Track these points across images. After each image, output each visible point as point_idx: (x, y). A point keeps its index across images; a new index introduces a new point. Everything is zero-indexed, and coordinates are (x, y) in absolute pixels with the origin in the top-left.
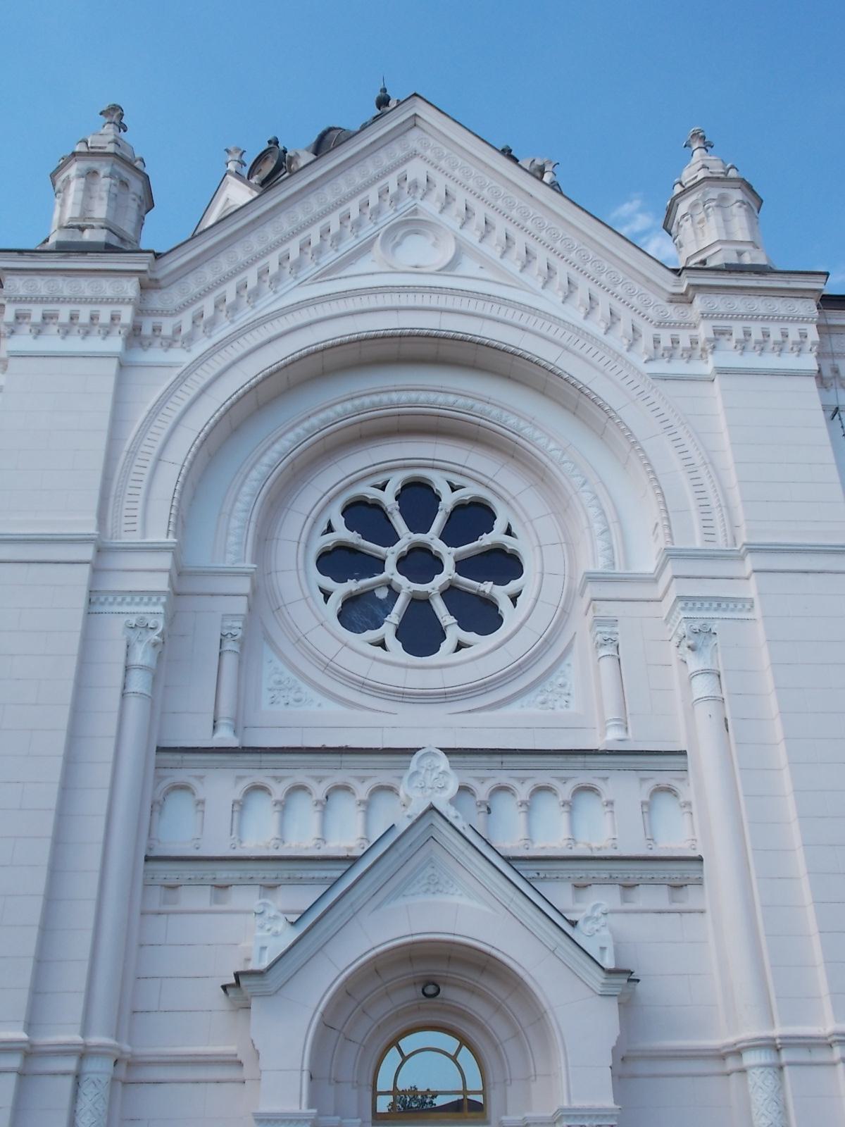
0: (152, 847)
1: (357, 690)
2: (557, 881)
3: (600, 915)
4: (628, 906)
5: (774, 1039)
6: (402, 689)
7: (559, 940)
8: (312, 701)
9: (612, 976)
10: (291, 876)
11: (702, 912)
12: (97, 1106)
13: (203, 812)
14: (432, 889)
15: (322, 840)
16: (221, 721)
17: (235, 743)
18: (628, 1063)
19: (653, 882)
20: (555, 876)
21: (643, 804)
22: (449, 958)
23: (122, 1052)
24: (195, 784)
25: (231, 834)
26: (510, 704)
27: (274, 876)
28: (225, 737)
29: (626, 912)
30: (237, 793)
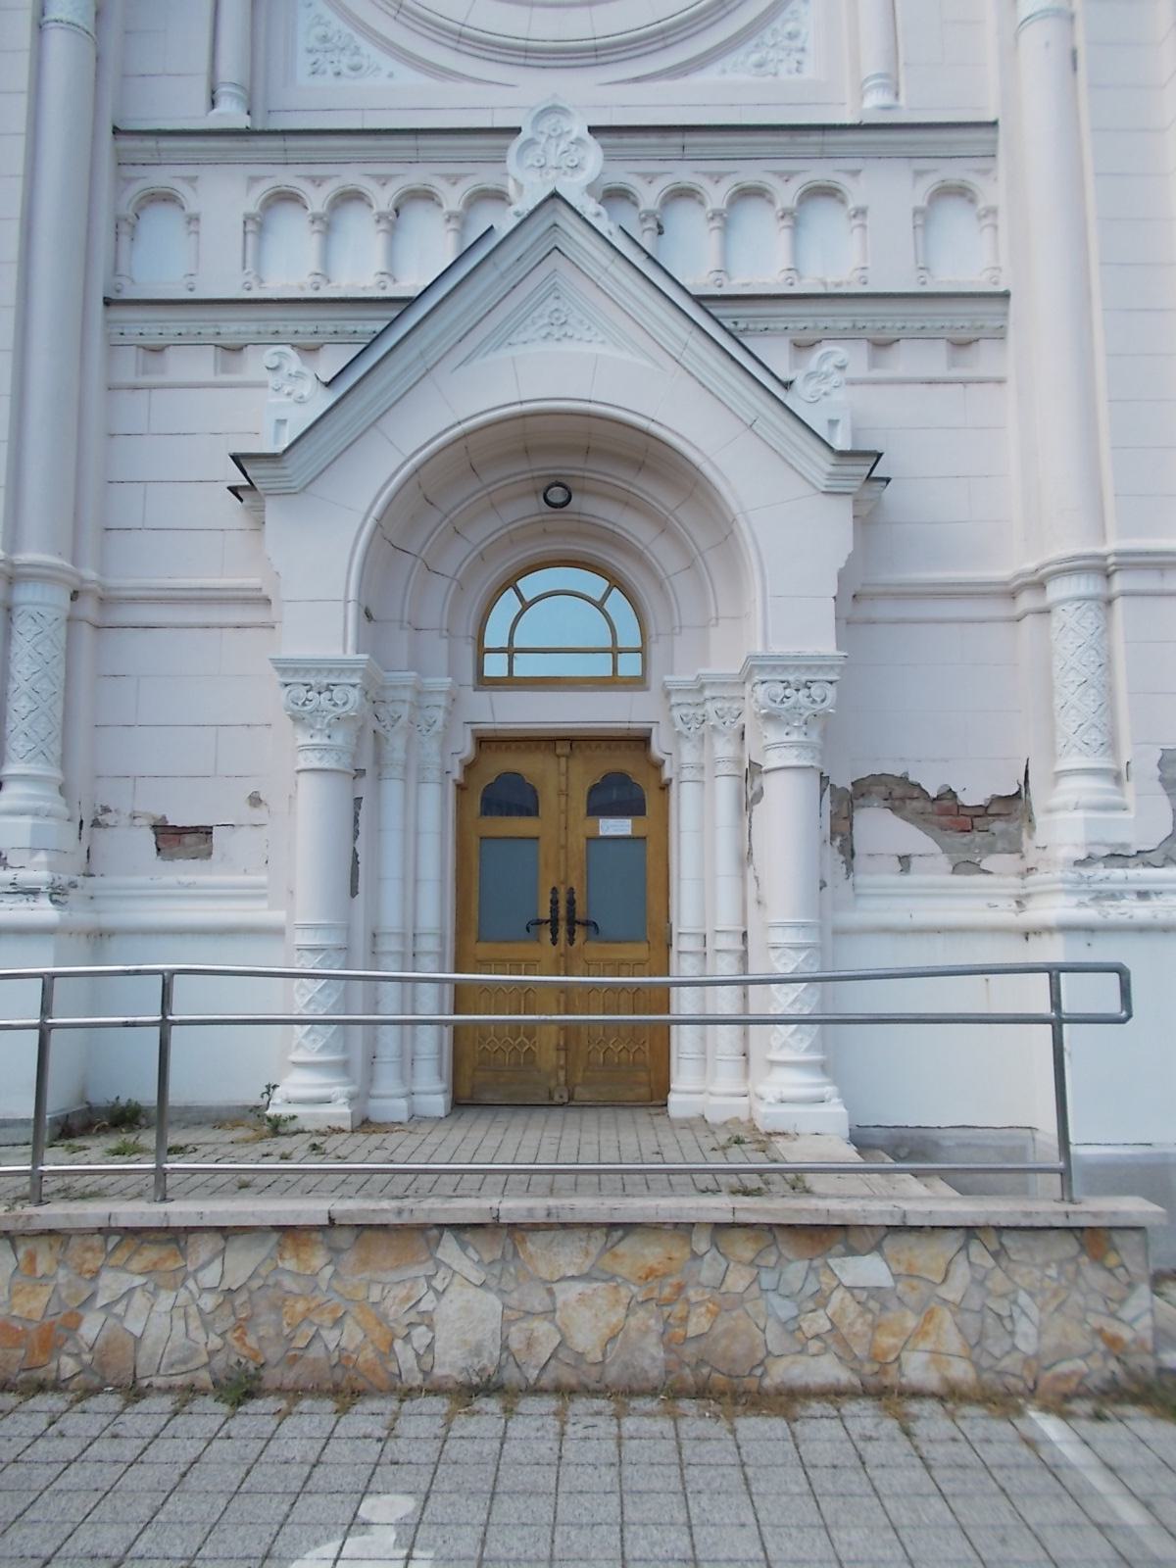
0: (119, 287)
1: (451, 48)
2: (766, 336)
3: (832, 369)
4: (877, 374)
5: (1105, 557)
6: (523, 42)
7: (758, 405)
8: (378, 69)
9: (846, 461)
10: (338, 329)
11: (1000, 381)
12: (40, 649)
13: (197, 233)
14: (557, 333)
15: (390, 274)
16: (222, 90)
17: (242, 122)
18: (859, 601)
19: (923, 335)
20: (762, 326)
21: (917, 212)
22: (588, 450)
23: (83, 581)
24: (183, 189)
25: (244, 268)
26: (702, 68)
27: (312, 329)
28: (230, 113)
29: (876, 382)
30: (251, 203)
